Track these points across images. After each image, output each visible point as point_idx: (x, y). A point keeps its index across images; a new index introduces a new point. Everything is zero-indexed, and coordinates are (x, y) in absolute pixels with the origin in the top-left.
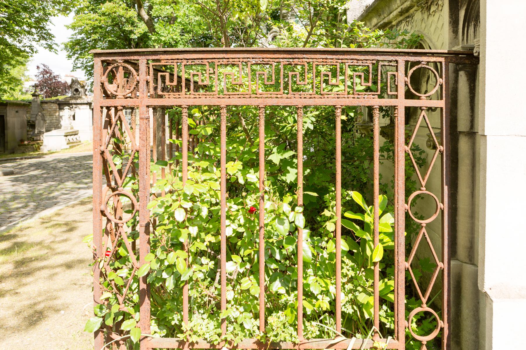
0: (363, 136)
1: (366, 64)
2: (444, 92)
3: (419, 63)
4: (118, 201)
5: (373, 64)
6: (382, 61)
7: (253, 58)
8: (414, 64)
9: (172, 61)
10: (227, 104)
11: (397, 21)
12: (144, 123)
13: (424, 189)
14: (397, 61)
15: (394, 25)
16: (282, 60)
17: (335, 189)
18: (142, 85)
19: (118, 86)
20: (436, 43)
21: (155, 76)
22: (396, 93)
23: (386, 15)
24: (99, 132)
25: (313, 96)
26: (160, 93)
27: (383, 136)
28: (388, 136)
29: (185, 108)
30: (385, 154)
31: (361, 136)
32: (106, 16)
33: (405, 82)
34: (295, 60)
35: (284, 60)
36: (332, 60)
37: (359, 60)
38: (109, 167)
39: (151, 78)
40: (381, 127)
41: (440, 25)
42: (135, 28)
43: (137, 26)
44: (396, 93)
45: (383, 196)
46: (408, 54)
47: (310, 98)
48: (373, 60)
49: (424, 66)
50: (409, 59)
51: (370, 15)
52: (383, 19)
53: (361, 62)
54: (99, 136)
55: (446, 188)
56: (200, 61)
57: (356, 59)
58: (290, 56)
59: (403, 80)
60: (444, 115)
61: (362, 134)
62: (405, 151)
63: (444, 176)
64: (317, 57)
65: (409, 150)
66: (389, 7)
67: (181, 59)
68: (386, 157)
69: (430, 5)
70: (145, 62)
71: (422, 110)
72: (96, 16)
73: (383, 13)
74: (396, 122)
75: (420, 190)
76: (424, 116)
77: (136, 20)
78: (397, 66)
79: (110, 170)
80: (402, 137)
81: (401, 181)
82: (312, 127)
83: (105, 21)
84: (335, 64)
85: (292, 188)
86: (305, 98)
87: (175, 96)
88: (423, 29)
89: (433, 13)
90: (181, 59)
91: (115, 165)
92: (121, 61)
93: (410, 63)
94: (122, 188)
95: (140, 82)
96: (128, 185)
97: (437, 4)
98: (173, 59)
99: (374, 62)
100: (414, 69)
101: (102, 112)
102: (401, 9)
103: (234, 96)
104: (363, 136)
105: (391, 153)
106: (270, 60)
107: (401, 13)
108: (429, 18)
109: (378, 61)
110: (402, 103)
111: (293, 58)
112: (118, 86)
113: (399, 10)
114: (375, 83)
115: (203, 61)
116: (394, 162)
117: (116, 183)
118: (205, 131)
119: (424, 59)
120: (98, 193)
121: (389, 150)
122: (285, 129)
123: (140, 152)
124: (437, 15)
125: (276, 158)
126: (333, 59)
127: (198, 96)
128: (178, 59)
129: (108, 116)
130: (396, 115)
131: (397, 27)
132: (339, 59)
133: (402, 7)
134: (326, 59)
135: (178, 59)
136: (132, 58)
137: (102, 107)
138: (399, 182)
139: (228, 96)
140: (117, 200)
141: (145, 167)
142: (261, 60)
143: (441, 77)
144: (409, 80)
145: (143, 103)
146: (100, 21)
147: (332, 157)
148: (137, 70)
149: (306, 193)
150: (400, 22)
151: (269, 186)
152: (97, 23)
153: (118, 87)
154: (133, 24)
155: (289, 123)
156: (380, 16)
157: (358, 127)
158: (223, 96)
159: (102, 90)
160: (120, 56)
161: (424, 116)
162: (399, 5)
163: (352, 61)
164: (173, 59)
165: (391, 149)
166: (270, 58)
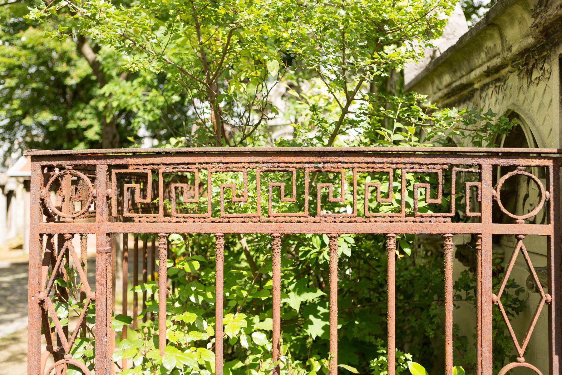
0: (429, 254)
1: (434, 171)
2: (552, 212)
3: (514, 167)
4: (62, 371)
5: (444, 170)
6: (458, 166)
7: (263, 163)
8: (505, 170)
9: (145, 167)
10: (226, 232)
11: (481, 83)
12: (104, 259)
13: (522, 359)
14: (480, 167)
15: (477, 89)
16: (307, 165)
17: (387, 350)
18: (100, 203)
19: (64, 199)
20: (541, 128)
21: (120, 187)
22: (479, 214)
23: (464, 73)
24: (37, 271)
25: (353, 219)
26: (126, 214)
27: (460, 260)
28: (468, 261)
29: (164, 237)
30: (463, 293)
31: (426, 254)
32: (28, 49)
33: (493, 197)
34: (326, 165)
35: (310, 165)
36: (382, 165)
37: (422, 164)
38: (51, 323)
39: (113, 192)
40: (457, 246)
41: (546, 101)
42: (73, 68)
43: (75, 65)
44: (479, 214)
45: (458, 369)
46: (495, 155)
47: (349, 222)
48: (444, 164)
49: (521, 172)
50: (498, 163)
51: (440, 69)
52: (460, 78)
53: (425, 167)
54: (37, 278)
55: (556, 359)
56: (186, 167)
57: (418, 163)
58: (319, 160)
59: (488, 193)
60: (553, 248)
61: (427, 251)
62: (493, 303)
63: (554, 341)
64: (359, 161)
65: (499, 301)
66: (469, 62)
67: (158, 165)
68: (464, 297)
69: (532, 69)
70: (105, 167)
71: (519, 239)
72: (13, 50)
73: (460, 69)
74: (479, 258)
75: (517, 361)
76: (521, 249)
77: (74, 56)
78: (480, 174)
79: (51, 326)
80: (488, 281)
81: (487, 348)
82: (349, 253)
83: (24, 58)
84: (386, 170)
85: (321, 347)
86: (342, 222)
87: (148, 220)
88: (521, 102)
89: (537, 81)
90: (158, 165)
91: (60, 319)
92: (71, 167)
93: (499, 168)
94: (70, 355)
95: (98, 198)
96: (78, 350)
97: (541, 69)
98: (146, 165)
99: (446, 167)
100: (507, 176)
101: (41, 241)
102: (488, 67)
103: (236, 220)
104: (429, 254)
105: (472, 291)
106: (289, 165)
107: (488, 73)
108: (531, 87)
109: (451, 166)
110: (487, 228)
111: (324, 163)
112: (64, 199)
113: (484, 68)
114: (447, 194)
115: (190, 166)
116: (476, 307)
117: (59, 343)
118: (191, 266)
119: (522, 162)
120: (35, 363)
121: (467, 286)
122: (308, 256)
123: (97, 303)
124: (542, 85)
125: (295, 301)
126: (383, 163)
127: (182, 220)
128: (153, 164)
129: (50, 245)
130: (479, 247)
131: (481, 93)
132: (392, 163)
133: (489, 64)
134: (373, 163)
135: (153, 164)
136: (86, 162)
137: (41, 235)
138: (484, 350)
139: (227, 220)
140: (60, 370)
141: (104, 325)
142: (276, 165)
143: (548, 189)
144: (498, 195)
145: (101, 230)
146: (20, 57)
147: (381, 290)
148: (93, 180)
149: (341, 366)
150: (484, 88)
151: (287, 354)
152: (14, 61)
153: (63, 201)
154: (69, 61)
155: (314, 248)
156: (455, 72)
157: (421, 240)
158: (220, 220)
159: (42, 210)
160: (69, 160)
161: (521, 249)
162: (485, 60)
163: (412, 166)
164: (146, 165)
165: (471, 285)
166: (290, 163)
